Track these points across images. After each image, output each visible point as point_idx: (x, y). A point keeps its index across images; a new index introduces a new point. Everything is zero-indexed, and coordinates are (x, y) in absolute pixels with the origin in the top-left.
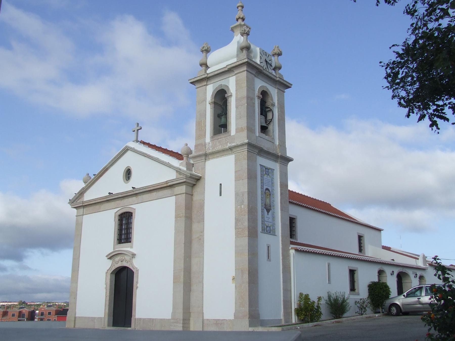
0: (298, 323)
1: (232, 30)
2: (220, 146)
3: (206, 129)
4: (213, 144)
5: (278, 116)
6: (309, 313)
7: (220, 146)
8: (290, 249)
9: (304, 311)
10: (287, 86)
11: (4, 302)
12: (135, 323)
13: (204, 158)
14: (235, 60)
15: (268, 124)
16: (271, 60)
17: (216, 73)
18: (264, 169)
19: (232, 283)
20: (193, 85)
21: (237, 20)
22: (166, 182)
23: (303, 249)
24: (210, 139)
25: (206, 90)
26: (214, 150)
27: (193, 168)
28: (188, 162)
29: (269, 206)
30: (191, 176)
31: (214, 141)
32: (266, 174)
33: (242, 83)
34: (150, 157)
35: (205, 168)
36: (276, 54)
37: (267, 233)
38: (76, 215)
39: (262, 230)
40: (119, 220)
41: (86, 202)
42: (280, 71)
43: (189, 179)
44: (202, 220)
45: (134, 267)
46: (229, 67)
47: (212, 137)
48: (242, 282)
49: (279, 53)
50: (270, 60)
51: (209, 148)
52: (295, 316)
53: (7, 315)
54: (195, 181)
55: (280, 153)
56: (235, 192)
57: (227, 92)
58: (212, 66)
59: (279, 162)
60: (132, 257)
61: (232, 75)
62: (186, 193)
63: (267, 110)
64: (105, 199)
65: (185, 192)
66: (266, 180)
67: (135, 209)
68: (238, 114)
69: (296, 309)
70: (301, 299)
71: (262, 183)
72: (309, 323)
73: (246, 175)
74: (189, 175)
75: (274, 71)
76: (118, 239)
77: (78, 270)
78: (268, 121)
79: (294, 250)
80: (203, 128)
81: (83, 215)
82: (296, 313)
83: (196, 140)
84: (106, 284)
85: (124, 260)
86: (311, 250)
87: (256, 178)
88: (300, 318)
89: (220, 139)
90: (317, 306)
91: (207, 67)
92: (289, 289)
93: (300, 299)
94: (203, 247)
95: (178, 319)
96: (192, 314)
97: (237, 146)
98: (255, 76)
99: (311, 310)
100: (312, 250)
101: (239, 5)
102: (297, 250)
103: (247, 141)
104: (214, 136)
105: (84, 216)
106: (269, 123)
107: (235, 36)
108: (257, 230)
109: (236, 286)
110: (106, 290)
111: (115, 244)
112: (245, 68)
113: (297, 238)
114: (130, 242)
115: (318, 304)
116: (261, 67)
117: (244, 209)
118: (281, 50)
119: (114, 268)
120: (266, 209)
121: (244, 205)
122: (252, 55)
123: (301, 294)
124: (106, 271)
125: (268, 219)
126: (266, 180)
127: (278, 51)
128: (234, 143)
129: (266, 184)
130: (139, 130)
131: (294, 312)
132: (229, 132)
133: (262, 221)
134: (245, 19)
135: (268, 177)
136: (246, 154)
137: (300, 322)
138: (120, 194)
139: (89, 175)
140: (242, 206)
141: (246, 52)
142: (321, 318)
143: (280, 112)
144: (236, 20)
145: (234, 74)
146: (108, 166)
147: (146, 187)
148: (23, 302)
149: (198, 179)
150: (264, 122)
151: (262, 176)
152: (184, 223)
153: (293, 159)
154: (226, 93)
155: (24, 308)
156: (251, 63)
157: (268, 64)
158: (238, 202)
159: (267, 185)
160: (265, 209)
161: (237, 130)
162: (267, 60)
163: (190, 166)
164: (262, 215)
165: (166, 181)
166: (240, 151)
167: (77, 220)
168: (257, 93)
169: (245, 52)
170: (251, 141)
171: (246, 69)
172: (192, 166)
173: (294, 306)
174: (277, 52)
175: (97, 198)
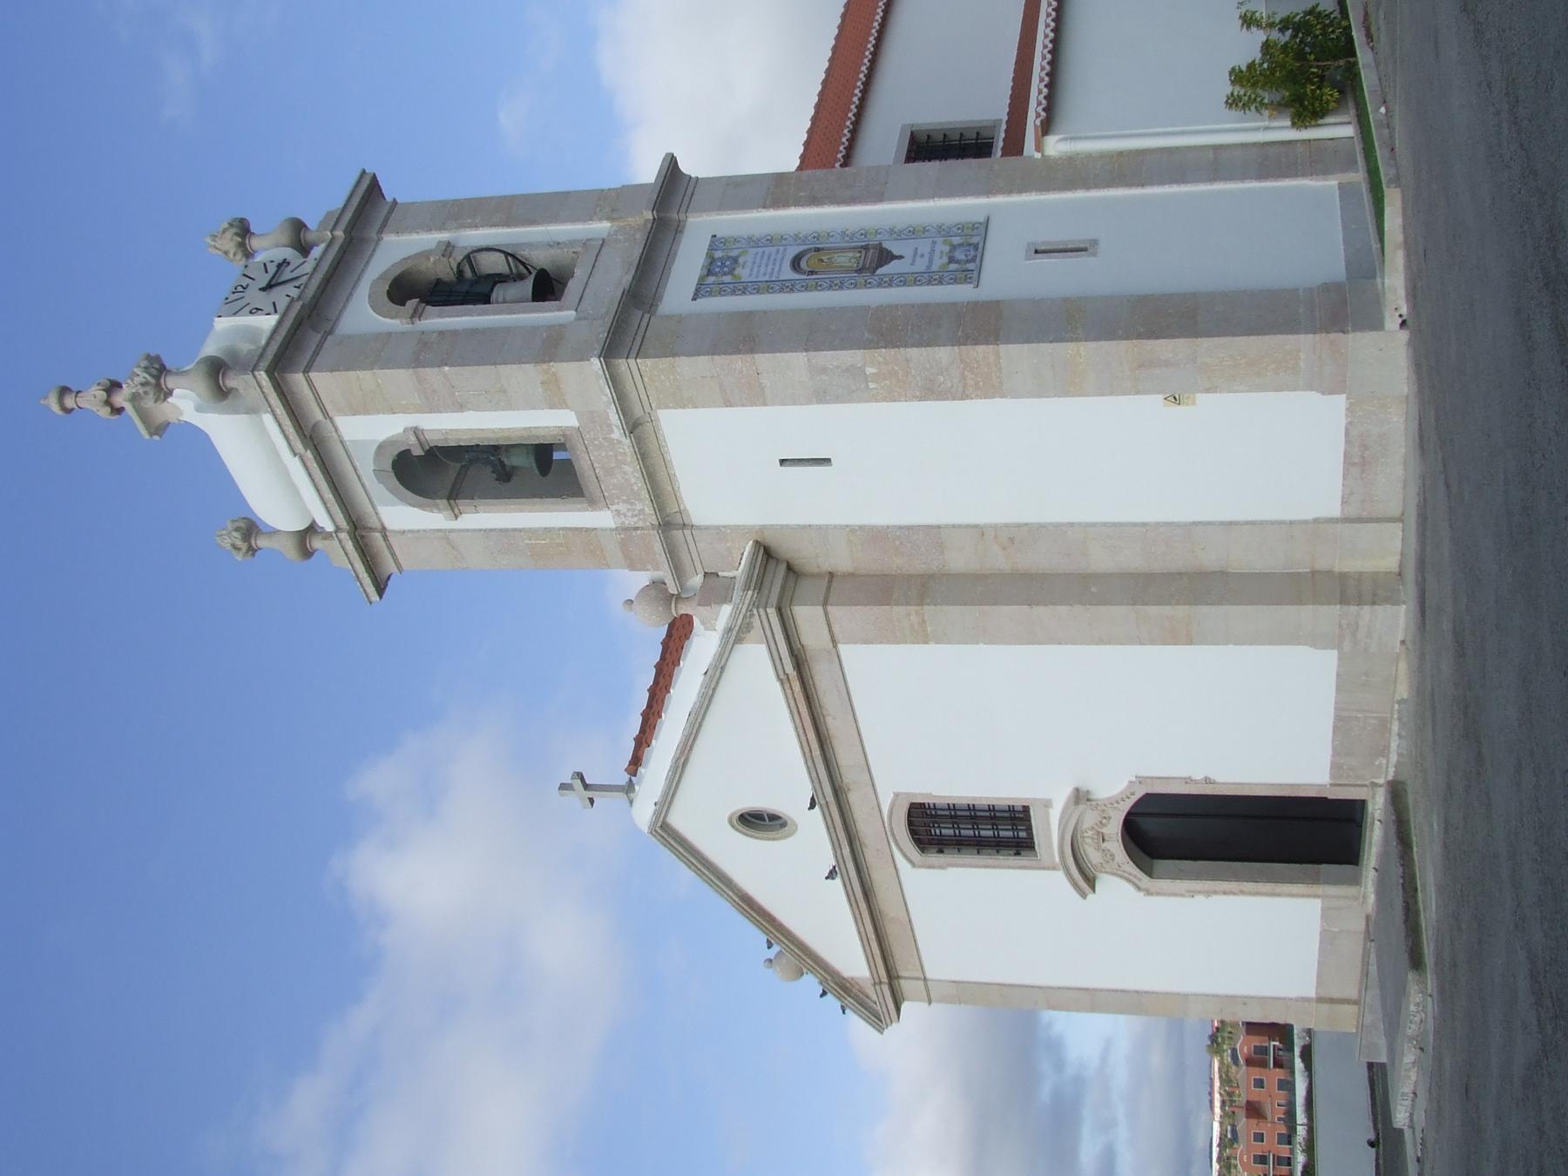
0: (1353, 112)
1: (159, 429)
2: (627, 468)
3: (563, 529)
4: (618, 498)
5: (491, 226)
6: (1311, 67)
7: (627, 468)
8: (1043, 156)
9: (1304, 86)
10: (370, 194)
11: (1211, 1102)
12: (1351, 785)
13: (678, 534)
14: (268, 419)
15: (528, 269)
16: (265, 265)
17: (329, 496)
18: (711, 279)
19: (1194, 403)
20: (389, 583)
21: (119, 411)
22: (782, 684)
23: (1041, 97)
24: (601, 509)
25: (404, 532)
26: (644, 494)
27: (720, 574)
28: (697, 598)
29: (864, 252)
30: (752, 588)
31: (606, 494)
32: (731, 272)
33: (361, 390)
34: (685, 745)
35: (717, 527)
36: (242, 245)
37: (978, 259)
38: (927, 1004)
39: (967, 280)
40: (941, 851)
41: (875, 972)
42: (312, 223)
43: (766, 592)
44: (934, 534)
45: (1128, 794)
46: (299, 446)
47: (593, 503)
48: (1187, 366)
49: (233, 230)
50: (266, 272)
51: (637, 512)
52: (1322, 125)
53: (1259, 1103)
54: (775, 563)
55: (642, 213)
56: (809, 402)
57: (402, 449)
58: (305, 510)
59: (682, 217)
60: (1088, 800)
61: (333, 430)
62: (825, 603)
63: (468, 273)
64: (863, 905)
65: (820, 609)
66: (758, 272)
67: (897, 795)
68: (490, 402)
69: (1294, 124)
70: (1251, 101)
71: (768, 287)
72: (1356, 64)
73: (738, 362)
74: (750, 593)
75: (312, 248)
76: (1017, 854)
77: (1137, 992)
78: (513, 268)
79: (1046, 137)
80: (558, 541)
81: (925, 979)
82: (1313, 123)
83: (609, 567)
84: (1192, 894)
85: (1098, 832)
86: (1045, 63)
87: (748, 316)
88: (1332, 105)
89: (597, 471)
90: (1281, 30)
91: (312, 529)
92: (1211, 155)
93: (1253, 108)
94: (1042, 526)
95: (1340, 626)
96: (1321, 565)
97: (621, 399)
98: (330, 332)
99: (1300, 56)
100: (1044, 58)
101: (56, 408)
102: (1046, 127)
103: (596, 364)
104: (586, 493)
105: (929, 975)
106: (521, 267)
107: (181, 418)
108: (968, 303)
109: (1208, 391)
110: (1215, 892)
111: (1033, 863)
112: (297, 379)
113: (990, 124)
114: (1026, 809)
115: (1271, 25)
116: (288, 308)
117: (879, 363)
118: (226, 226)
119: (1131, 868)
120: (877, 268)
121: (864, 365)
122: (245, 347)
123: (1233, 102)
124: (1142, 894)
125: (922, 256)
126: (758, 272)
127: (229, 235)
128: (608, 416)
129: (773, 269)
130: (588, 782)
131: (1309, 129)
132: (564, 435)
133: (929, 283)
134: (112, 378)
135: (745, 262)
136: (649, 362)
137: (1351, 104)
138: (839, 852)
139: (772, 958)
140: (868, 373)
141: (231, 374)
142: (1331, 13)
143: (477, 221)
144: (116, 417)
145: (328, 420)
146: (731, 894)
147: (808, 755)
148: (1212, 1043)
149: (766, 554)
150: (519, 285)
151: (741, 289)
152: (946, 608)
153: (667, 154)
154: (408, 451)
155: (1234, 1051)
156: (275, 355)
157: (280, 281)
158: (853, 391)
159: (777, 265)
160: (878, 272)
161: (556, 400)
162: (263, 284)
163: (715, 589)
164: (905, 283)
165: (778, 684)
166: (640, 386)
167: (946, 999)
168: (396, 322)
169: (232, 381)
170: (596, 345)
171: (301, 374)
172: (715, 578)
173: (1282, 130)
174: (232, 240)
175: (859, 933)
